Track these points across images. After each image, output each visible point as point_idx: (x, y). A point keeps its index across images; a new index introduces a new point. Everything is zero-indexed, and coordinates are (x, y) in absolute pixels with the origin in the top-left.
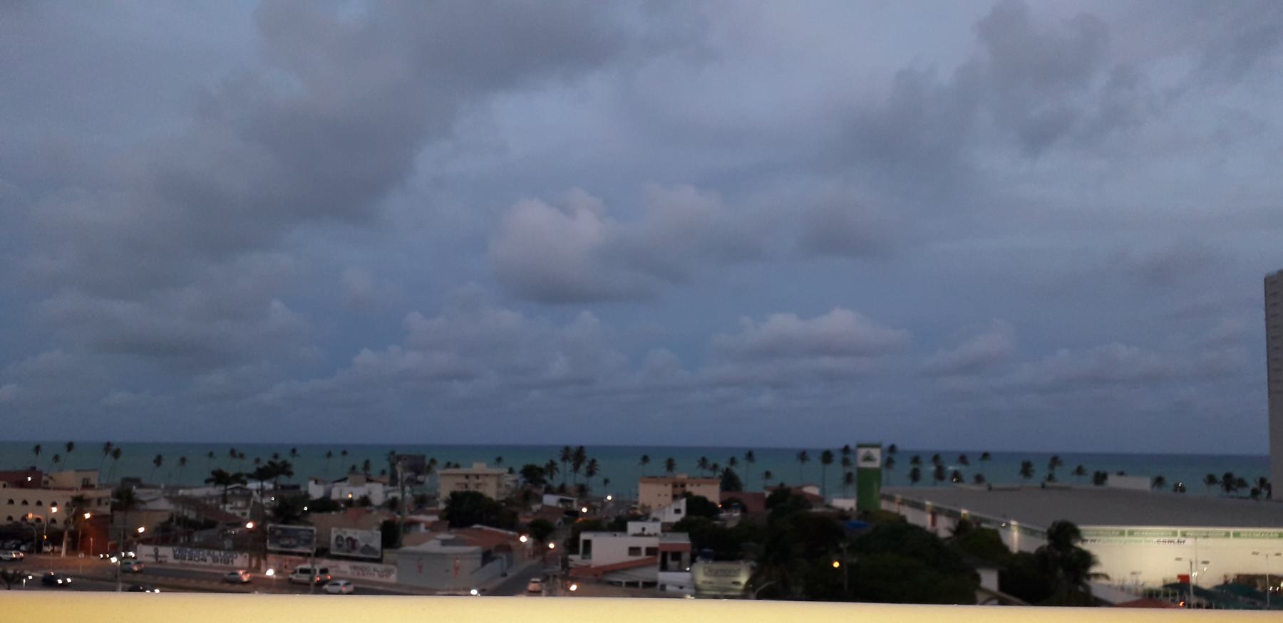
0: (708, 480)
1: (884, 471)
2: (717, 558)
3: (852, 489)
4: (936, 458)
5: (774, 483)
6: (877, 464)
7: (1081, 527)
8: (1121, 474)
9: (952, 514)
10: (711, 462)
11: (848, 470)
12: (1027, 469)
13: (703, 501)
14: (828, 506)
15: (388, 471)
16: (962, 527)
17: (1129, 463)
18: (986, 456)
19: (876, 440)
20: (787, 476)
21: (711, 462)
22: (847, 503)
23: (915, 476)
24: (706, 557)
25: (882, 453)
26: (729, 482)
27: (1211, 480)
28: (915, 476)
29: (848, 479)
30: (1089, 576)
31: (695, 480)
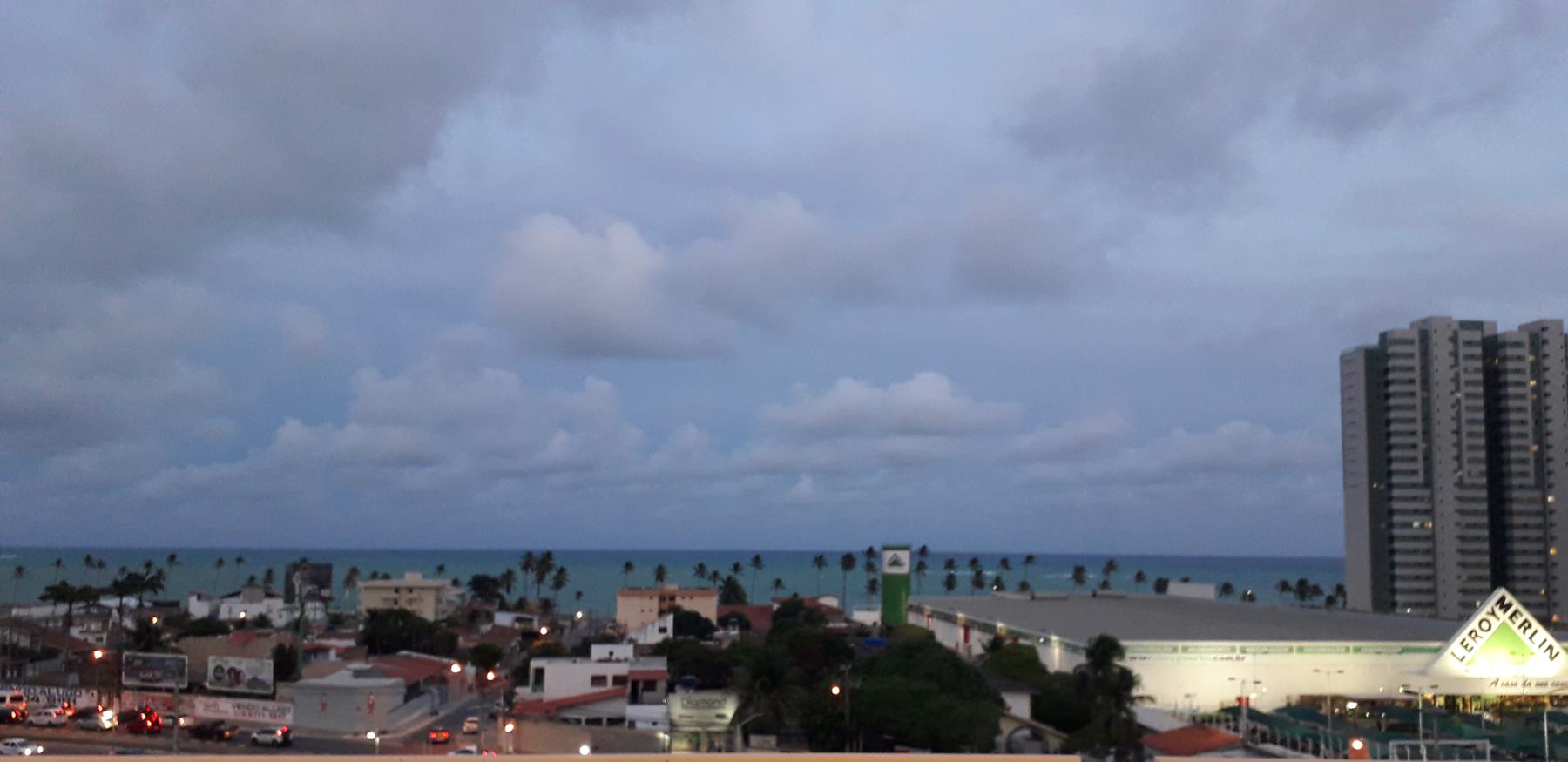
0: (703, 591)
2: (701, 687)
3: (877, 598)
4: (974, 562)
5: (785, 594)
6: (905, 570)
7: (1124, 643)
8: (1186, 580)
9: (987, 628)
11: (872, 576)
12: (1079, 574)
14: (848, 621)
16: (995, 645)
17: (1192, 568)
18: (1029, 559)
20: (801, 584)
21: (710, 570)
22: (869, 617)
23: (950, 583)
24: (687, 685)
25: (912, 556)
26: (731, 593)
27: (1284, 586)
28: (950, 583)
29: (872, 586)
30: (1132, 700)
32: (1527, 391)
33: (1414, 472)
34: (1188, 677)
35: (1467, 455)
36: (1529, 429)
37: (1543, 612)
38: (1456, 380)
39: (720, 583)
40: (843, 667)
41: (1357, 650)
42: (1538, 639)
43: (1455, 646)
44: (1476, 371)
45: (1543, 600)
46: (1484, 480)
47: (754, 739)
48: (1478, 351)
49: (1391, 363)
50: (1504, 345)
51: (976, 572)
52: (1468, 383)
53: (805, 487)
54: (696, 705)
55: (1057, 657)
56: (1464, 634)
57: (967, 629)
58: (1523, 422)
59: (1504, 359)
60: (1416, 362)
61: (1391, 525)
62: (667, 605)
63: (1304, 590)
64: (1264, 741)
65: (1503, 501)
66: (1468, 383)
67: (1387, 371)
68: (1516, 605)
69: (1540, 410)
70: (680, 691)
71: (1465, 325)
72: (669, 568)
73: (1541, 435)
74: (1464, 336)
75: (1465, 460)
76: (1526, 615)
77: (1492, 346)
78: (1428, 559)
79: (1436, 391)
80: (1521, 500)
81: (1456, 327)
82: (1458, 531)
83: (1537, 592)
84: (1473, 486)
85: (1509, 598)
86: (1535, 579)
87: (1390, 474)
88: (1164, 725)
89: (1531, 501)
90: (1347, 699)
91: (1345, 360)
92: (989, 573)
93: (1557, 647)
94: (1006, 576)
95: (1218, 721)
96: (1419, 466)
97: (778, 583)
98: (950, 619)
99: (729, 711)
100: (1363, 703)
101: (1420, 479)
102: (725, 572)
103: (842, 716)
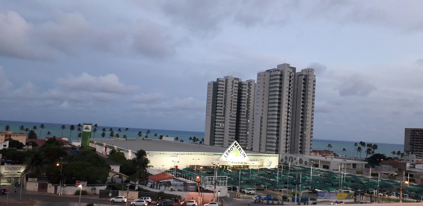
0: (22, 134)
1: (92, 133)
2: (13, 164)
3: (80, 139)
4: (111, 129)
5: (51, 136)
6: (90, 131)
7: (147, 152)
8: (167, 136)
9: (110, 147)
10: (25, 128)
11: (80, 132)
12: (140, 134)
13: (17, 142)
14: (70, 145)
15: (331, 149)
16: (113, 152)
17: (169, 133)
18: (127, 129)
19: (90, 123)
20: (56, 134)
21: (25, 128)
22: (77, 144)
23: (103, 135)
24: (8, 163)
25: (92, 127)
26: (32, 135)
27: (191, 139)
28: (103, 135)
29: (80, 135)
30: (147, 167)
31: (15, 134)
32: (246, 96)
33: (222, 113)
34: (162, 161)
35: (233, 109)
36: (246, 105)
37: (244, 147)
38: (232, 92)
39: (28, 132)
40: (61, 158)
41: (204, 154)
42: (242, 153)
43: (225, 154)
44: (237, 90)
45: (245, 144)
46: (236, 116)
47: (29, 179)
48: (237, 85)
49: (219, 86)
50: (243, 84)
51: (113, 132)
52: (235, 93)
53: (65, 105)
54: (10, 169)
55: (130, 156)
56: (227, 151)
57: (106, 148)
58: (245, 103)
59: (242, 88)
60: (224, 86)
61: (215, 125)
62: (8, 138)
63: (195, 140)
64: (179, 177)
65: (239, 121)
66: (235, 93)
67: (218, 88)
68: (238, 145)
69: (248, 100)
70: (6, 165)
71: (236, 79)
72: (10, 127)
73: (248, 106)
74: (235, 81)
75: (232, 111)
76: (240, 147)
77: (240, 85)
78: (222, 133)
79: (228, 94)
80: (243, 120)
81: (233, 79)
82: (229, 127)
83: (244, 142)
84: (233, 117)
85: (237, 143)
86: (244, 139)
87: (216, 113)
88: (154, 173)
89: (245, 121)
90: (201, 166)
91: (209, 84)
92: (115, 133)
93: (246, 155)
94: (119, 133)
95: (169, 172)
96: (222, 111)
97: (49, 133)
98: (101, 145)
99: (22, 170)
100: (204, 167)
101: (222, 114)
102: (30, 129)
103: (59, 172)
